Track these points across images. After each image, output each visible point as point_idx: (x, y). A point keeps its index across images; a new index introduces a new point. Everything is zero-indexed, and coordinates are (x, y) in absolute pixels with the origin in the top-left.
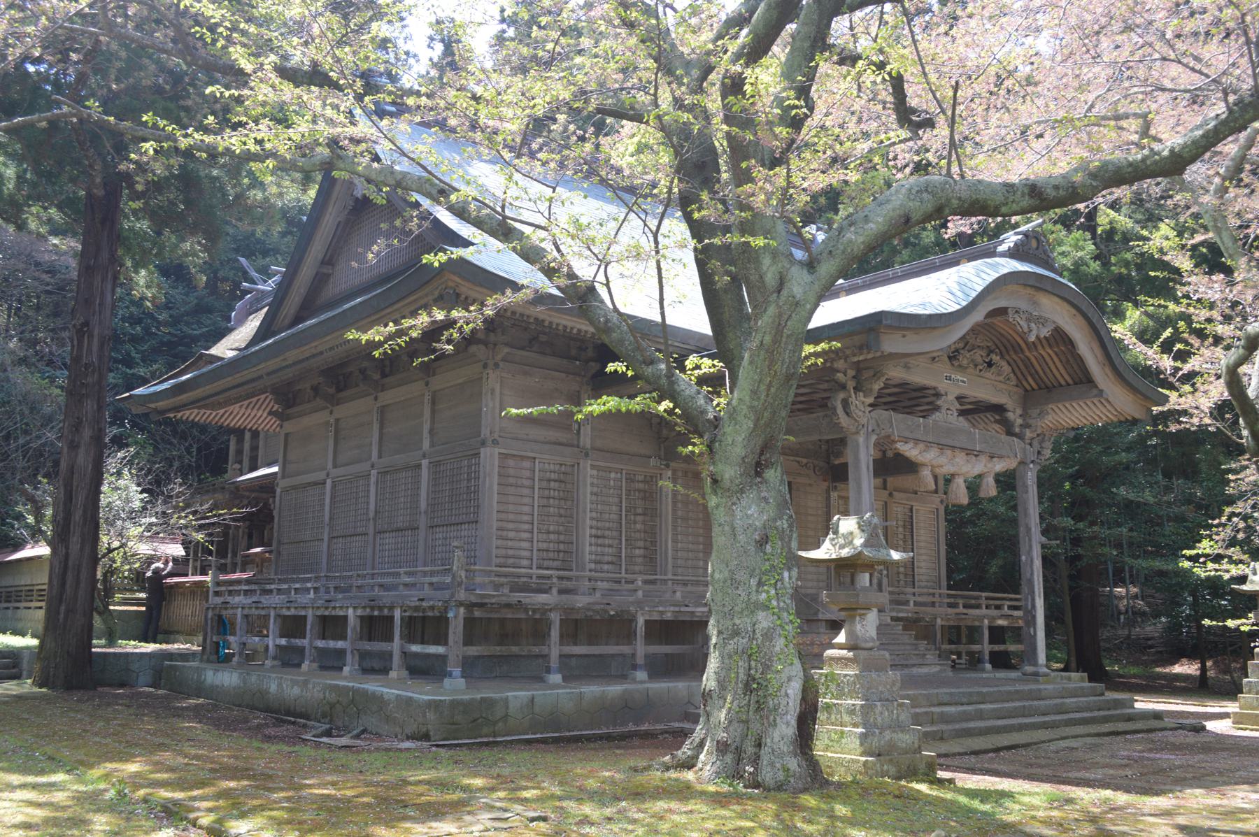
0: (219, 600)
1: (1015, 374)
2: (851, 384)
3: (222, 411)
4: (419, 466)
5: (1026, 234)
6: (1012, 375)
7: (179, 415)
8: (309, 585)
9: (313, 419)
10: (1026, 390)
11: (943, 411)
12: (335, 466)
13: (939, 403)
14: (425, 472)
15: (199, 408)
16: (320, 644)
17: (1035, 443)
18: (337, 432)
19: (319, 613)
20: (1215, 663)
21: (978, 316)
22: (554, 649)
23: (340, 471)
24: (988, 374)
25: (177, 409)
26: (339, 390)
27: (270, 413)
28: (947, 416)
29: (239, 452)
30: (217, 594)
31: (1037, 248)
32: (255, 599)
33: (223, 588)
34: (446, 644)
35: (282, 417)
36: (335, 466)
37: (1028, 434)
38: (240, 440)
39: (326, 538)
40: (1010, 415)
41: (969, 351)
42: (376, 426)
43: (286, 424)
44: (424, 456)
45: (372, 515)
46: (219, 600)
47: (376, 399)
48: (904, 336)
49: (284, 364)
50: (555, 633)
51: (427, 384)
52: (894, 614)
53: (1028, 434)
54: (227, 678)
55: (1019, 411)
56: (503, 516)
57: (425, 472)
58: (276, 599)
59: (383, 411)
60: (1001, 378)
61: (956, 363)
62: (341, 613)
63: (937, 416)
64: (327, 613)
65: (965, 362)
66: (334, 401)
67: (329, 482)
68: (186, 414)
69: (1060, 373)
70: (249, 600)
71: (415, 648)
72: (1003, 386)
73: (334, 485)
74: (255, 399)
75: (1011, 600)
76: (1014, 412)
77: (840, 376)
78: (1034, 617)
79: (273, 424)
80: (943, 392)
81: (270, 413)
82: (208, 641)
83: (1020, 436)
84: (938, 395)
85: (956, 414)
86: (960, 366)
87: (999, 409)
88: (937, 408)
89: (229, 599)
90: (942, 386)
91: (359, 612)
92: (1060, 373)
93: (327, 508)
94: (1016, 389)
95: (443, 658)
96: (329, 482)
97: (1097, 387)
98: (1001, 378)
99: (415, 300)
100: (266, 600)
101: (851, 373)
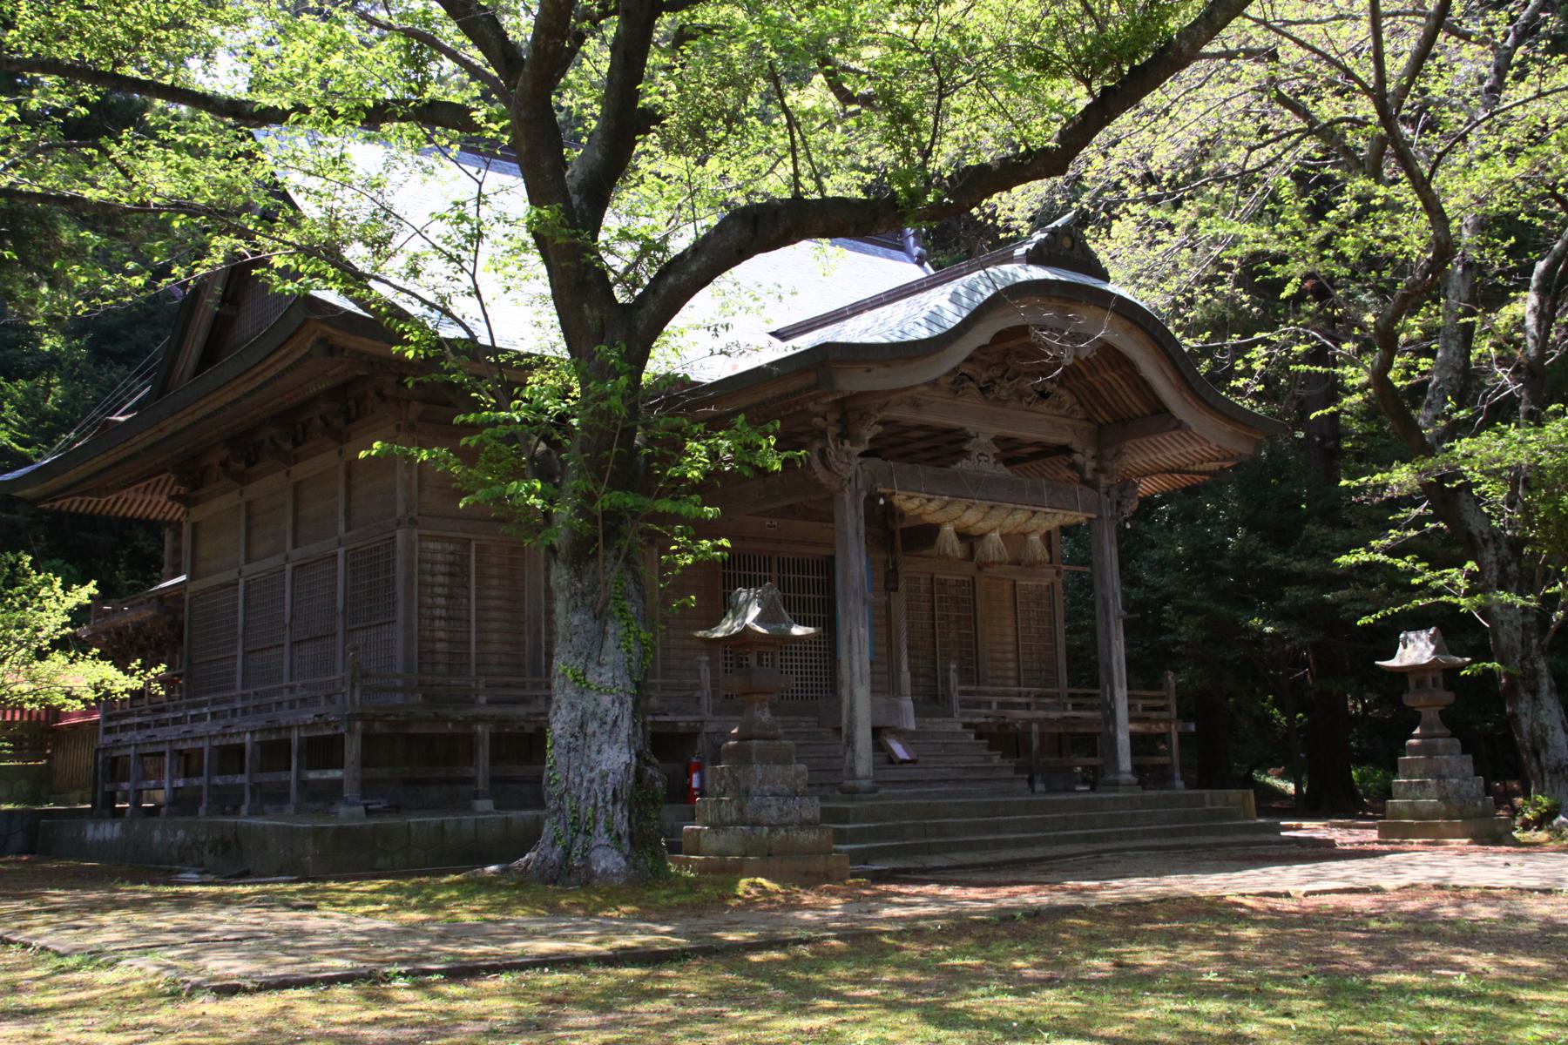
0: (109, 739)
1: (1082, 405)
2: (833, 431)
3: (113, 498)
4: (335, 555)
5: (1054, 232)
6: (1077, 407)
7: (57, 505)
8: (205, 710)
9: (222, 504)
10: (1100, 425)
11: (973, 456)
12: (248, 561)
13: (966, 447)
14: (341, 562)
15: (81, 494)
16: (218, 780)
17: (1114, 492)
18: (249, 517)
19: (216, 743)
20: (1192, 734)
21: (982, 336)
22: (482, 769)
23: (253, 567)
24: (1043, 406)
25: (51, 496)
26: (250, 464)
27: (171, 498)
28: (981, 462)
29: (177, 551)
30: (108, 731)
31: (1073, 247)
32: (149, 732)
33: (114, 723)
34: (341, 766)
35: (187, 501)
36: (248, 561)
37: (1103, 480)
38: (178, 535)
39: (240, 653)
40: (1078, 458)
41: (1009, 380)
42: (289, 510)
43: (193, 510)
44: (340, 544)
45: (287, 620)
46: (109, 739)
47: (288, 474)
48: (869, 370)
49: (164, 435)
50: (484, 752)
51: (340, 453)
52: (967, 720)
53: (1103, 480)
54: (109, 831)
55: (1090, 452)
56: (1161, 703)
57: (341, 562)
58: (171, 732)
59: (297, 487)
60: (1063, 411)
61: (991, 397)
62: (237, 740)
63: (963, 465)
64: (224, 742)
65: (1004, 394)
66: (243, 479)
67: (242, 581)
68: (64, 504)
69: (1137, 405)
70: (139, 737)
71: (312, 775)
72: (1067, 421)
73: (247, 586)
74: (154, 480)
75: (1143, 698)
76: (1083, 454)
77: (817, 420)
78: (1113, 712)
79: (176, 512)
80: (972, 433)
81: (171, 498)
82: (99, 794)
83: (1092, 485)
84: (967, 438)
85: (993, 460)
86: (998, 399)
87: (1066, 450)
88: (965, 454)
89: (121, 736)
90: (971, 427)
91: (258, 737)
92: (1137, 405)
93: (240, 616)
94: (1085, 424)
95: (338, 783)
96: (242, 581)
97: (1173, 417)
98: (1063, 411)
99: (287, 355)
100: (160, 734)
101: (832, 417)
